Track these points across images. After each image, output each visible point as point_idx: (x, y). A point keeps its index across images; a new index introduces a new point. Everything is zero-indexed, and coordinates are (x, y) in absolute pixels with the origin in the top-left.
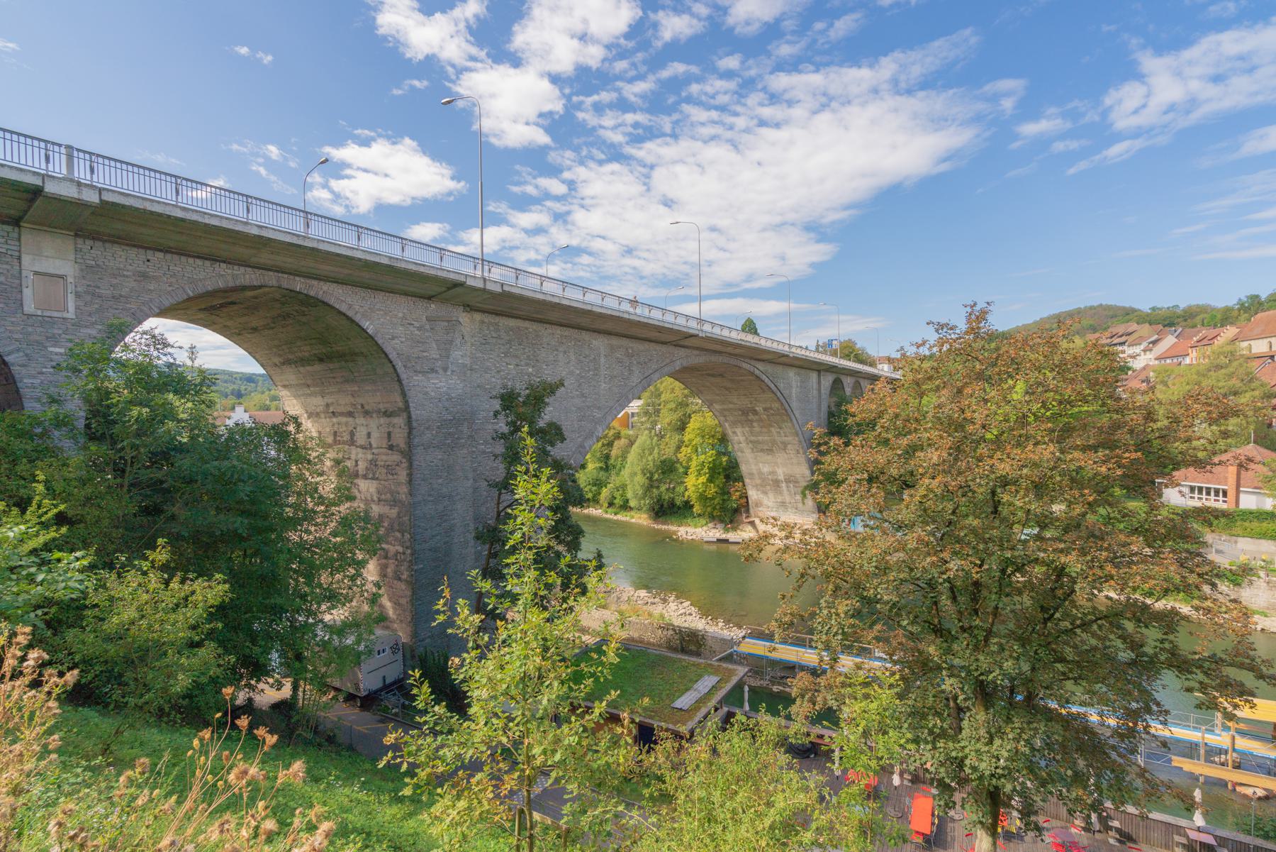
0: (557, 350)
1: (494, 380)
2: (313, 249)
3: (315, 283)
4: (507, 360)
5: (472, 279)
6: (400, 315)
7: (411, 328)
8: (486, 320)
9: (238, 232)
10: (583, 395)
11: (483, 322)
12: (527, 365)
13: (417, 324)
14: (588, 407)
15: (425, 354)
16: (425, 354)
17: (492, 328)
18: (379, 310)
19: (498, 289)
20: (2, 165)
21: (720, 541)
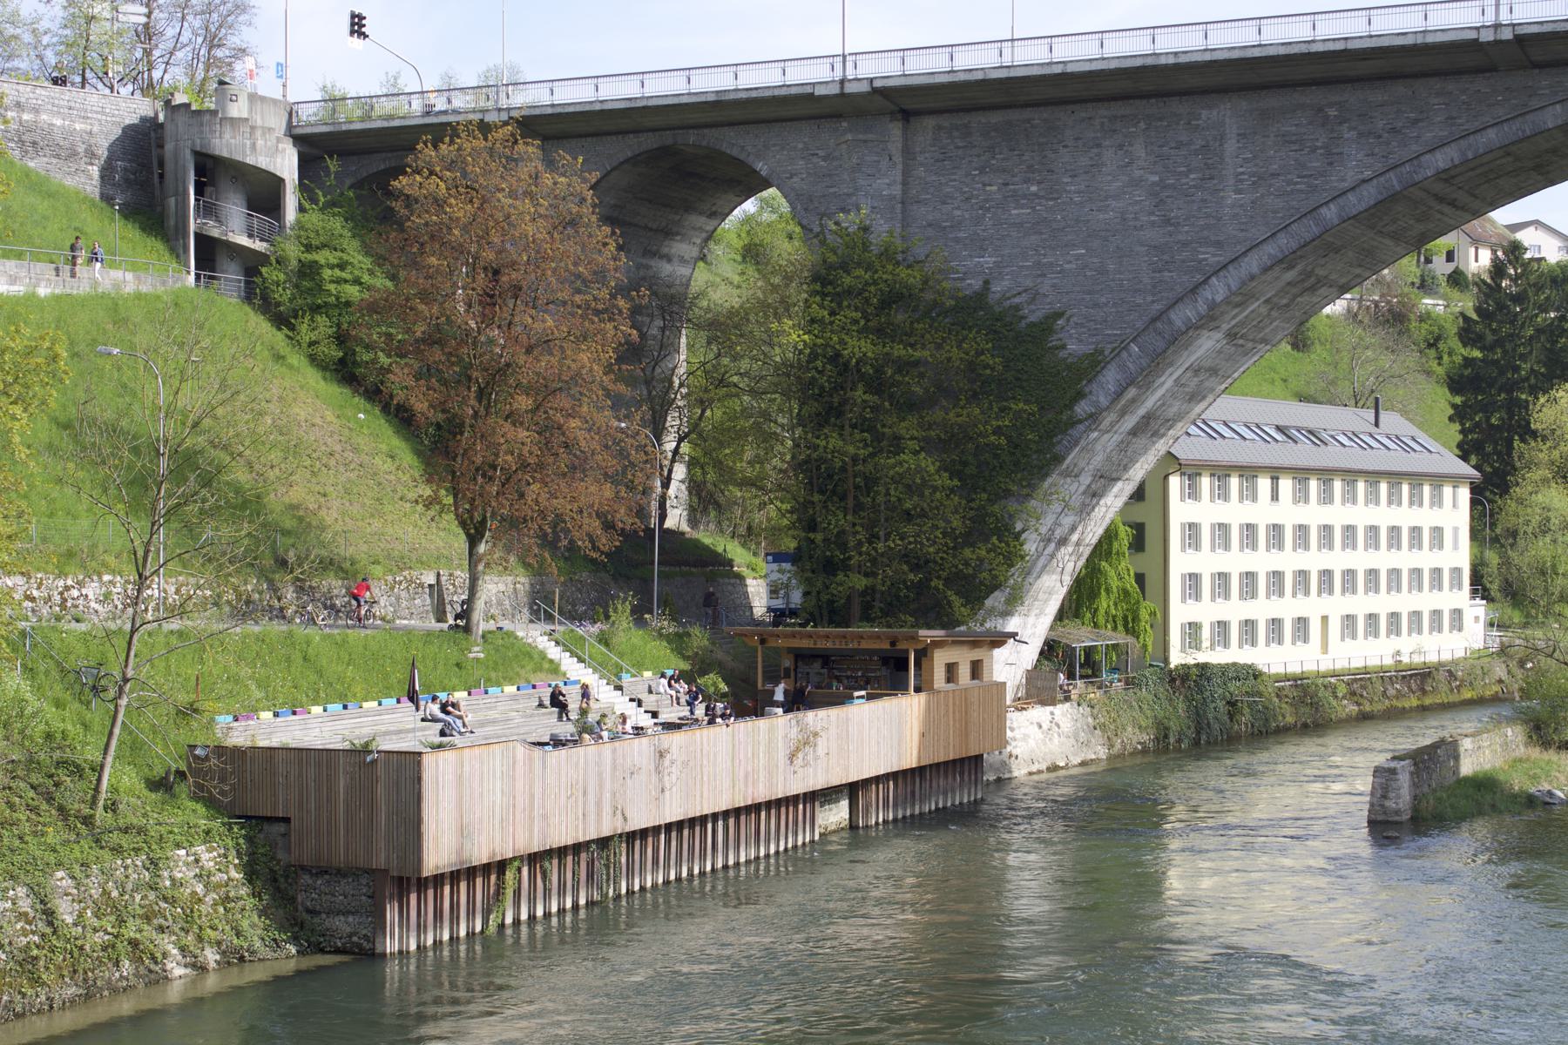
0: (1098, 146)
1: (958, 213)
2: (644, 107)
3: (706, 131)
4: (986, 179)
5: (823, 86)
6: (800, 146)
7: (815, 160)
8: (946, 124)
9: (560, 114)
10: (1167, 221)
11: (940, 128)
12: (1027, 181)
13: (821, 153)
14: (1185, 244)
15: (832, 190)
16: (832, 190)
17: (956, 134)
18: (774, 145)
19: (865, 87)
20: (1497, 5)
21: (399, 1025)
